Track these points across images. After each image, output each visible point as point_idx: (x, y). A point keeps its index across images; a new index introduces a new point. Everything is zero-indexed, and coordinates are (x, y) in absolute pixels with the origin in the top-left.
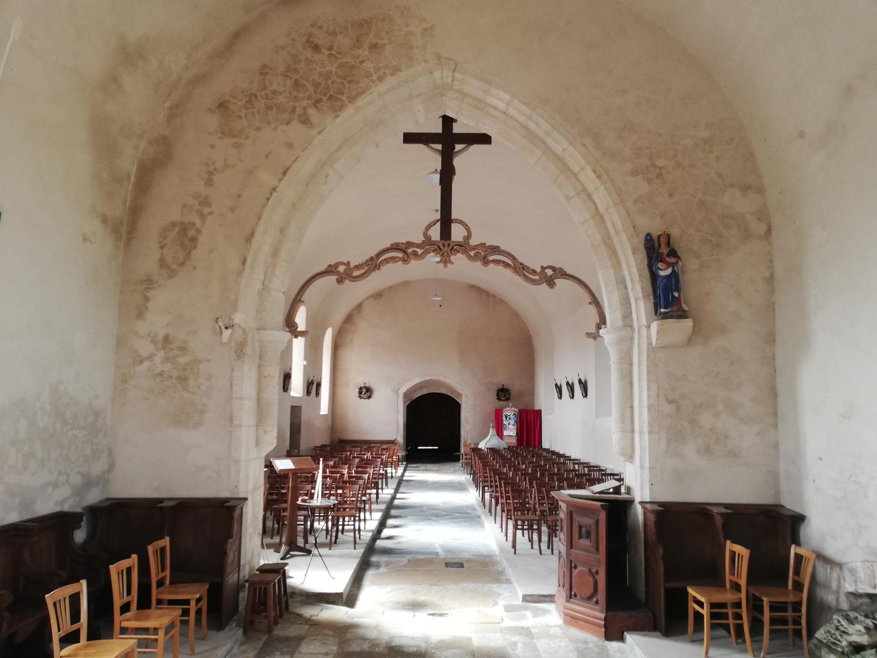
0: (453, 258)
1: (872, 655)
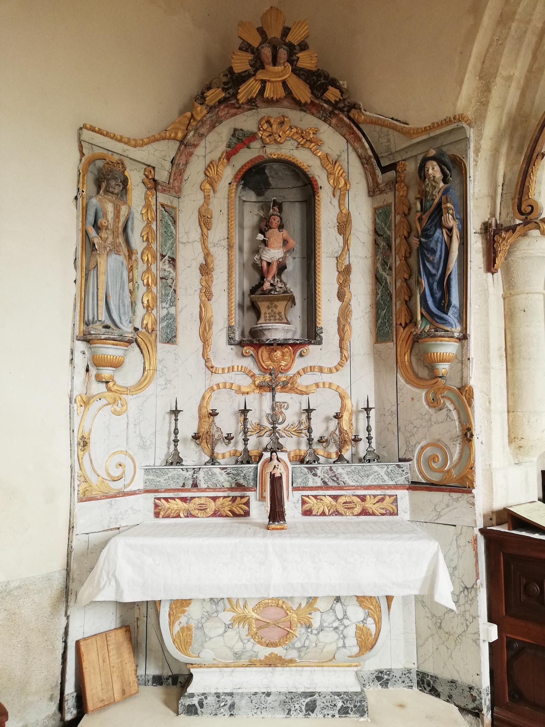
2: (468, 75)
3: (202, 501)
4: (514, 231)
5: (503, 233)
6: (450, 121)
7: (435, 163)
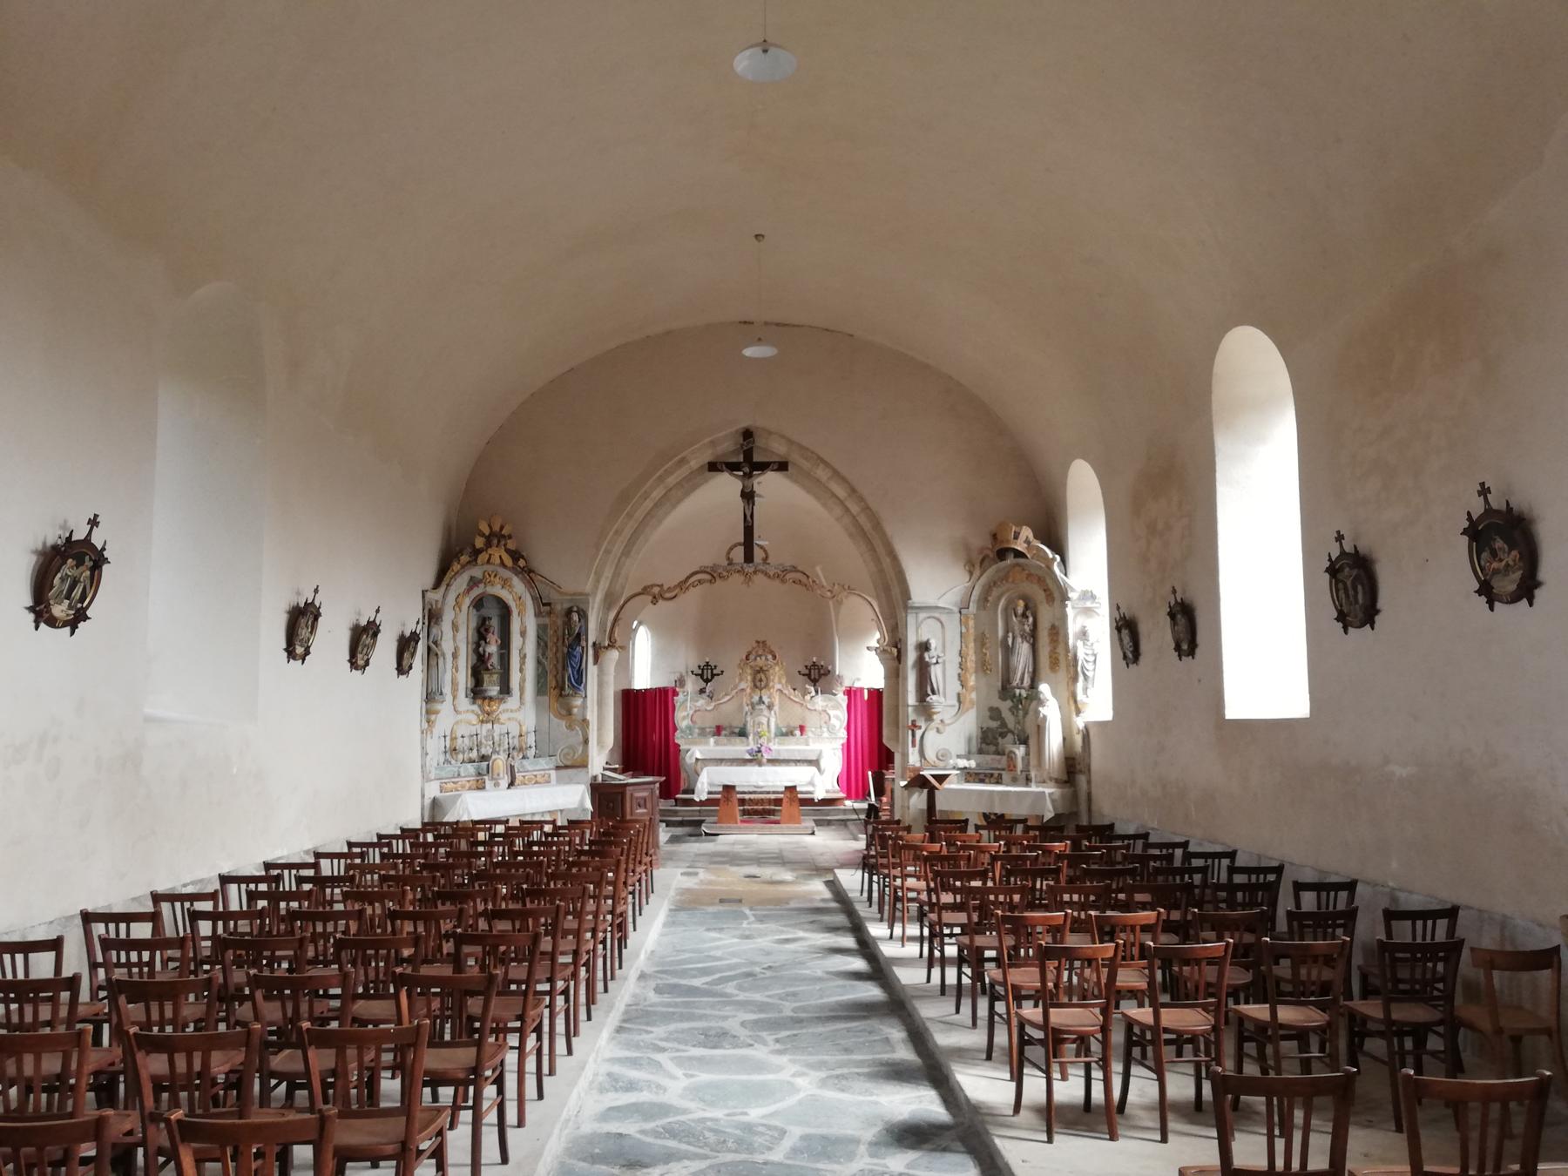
3: (464, 783)
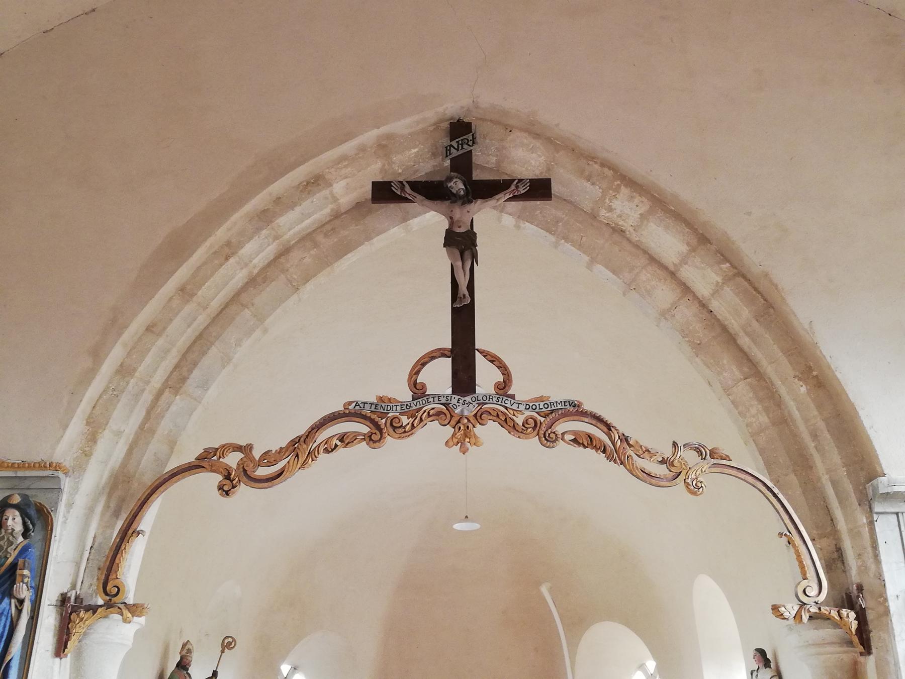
0: (479, 430)
1: (483, 168)
2: (75, 420)
4: (94, 613)
5: (82, 612)
6: (45, 467)
7: (17, 513)
